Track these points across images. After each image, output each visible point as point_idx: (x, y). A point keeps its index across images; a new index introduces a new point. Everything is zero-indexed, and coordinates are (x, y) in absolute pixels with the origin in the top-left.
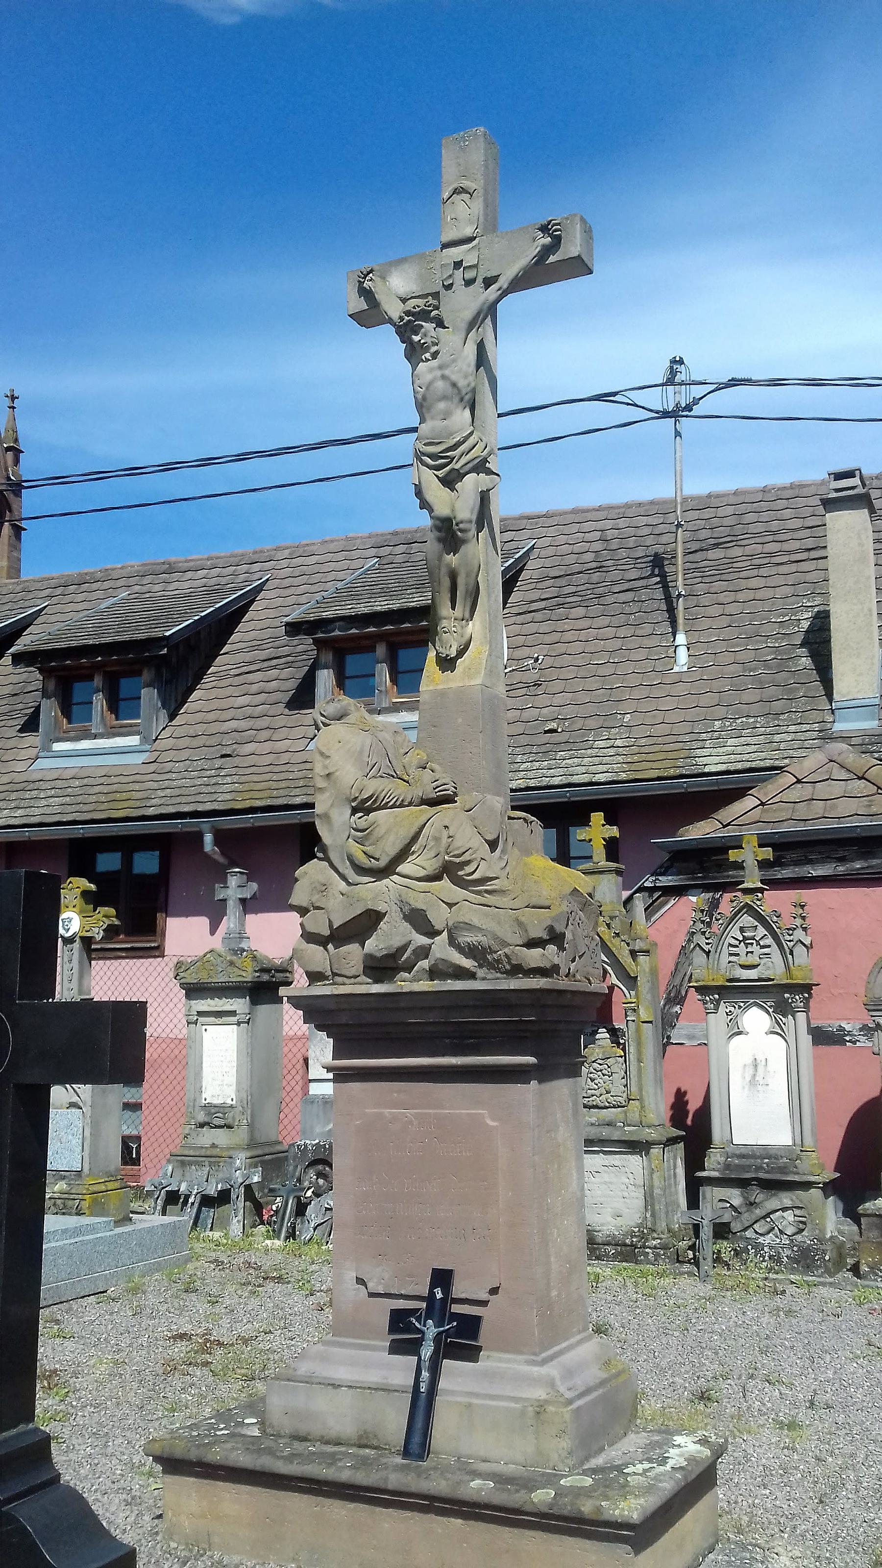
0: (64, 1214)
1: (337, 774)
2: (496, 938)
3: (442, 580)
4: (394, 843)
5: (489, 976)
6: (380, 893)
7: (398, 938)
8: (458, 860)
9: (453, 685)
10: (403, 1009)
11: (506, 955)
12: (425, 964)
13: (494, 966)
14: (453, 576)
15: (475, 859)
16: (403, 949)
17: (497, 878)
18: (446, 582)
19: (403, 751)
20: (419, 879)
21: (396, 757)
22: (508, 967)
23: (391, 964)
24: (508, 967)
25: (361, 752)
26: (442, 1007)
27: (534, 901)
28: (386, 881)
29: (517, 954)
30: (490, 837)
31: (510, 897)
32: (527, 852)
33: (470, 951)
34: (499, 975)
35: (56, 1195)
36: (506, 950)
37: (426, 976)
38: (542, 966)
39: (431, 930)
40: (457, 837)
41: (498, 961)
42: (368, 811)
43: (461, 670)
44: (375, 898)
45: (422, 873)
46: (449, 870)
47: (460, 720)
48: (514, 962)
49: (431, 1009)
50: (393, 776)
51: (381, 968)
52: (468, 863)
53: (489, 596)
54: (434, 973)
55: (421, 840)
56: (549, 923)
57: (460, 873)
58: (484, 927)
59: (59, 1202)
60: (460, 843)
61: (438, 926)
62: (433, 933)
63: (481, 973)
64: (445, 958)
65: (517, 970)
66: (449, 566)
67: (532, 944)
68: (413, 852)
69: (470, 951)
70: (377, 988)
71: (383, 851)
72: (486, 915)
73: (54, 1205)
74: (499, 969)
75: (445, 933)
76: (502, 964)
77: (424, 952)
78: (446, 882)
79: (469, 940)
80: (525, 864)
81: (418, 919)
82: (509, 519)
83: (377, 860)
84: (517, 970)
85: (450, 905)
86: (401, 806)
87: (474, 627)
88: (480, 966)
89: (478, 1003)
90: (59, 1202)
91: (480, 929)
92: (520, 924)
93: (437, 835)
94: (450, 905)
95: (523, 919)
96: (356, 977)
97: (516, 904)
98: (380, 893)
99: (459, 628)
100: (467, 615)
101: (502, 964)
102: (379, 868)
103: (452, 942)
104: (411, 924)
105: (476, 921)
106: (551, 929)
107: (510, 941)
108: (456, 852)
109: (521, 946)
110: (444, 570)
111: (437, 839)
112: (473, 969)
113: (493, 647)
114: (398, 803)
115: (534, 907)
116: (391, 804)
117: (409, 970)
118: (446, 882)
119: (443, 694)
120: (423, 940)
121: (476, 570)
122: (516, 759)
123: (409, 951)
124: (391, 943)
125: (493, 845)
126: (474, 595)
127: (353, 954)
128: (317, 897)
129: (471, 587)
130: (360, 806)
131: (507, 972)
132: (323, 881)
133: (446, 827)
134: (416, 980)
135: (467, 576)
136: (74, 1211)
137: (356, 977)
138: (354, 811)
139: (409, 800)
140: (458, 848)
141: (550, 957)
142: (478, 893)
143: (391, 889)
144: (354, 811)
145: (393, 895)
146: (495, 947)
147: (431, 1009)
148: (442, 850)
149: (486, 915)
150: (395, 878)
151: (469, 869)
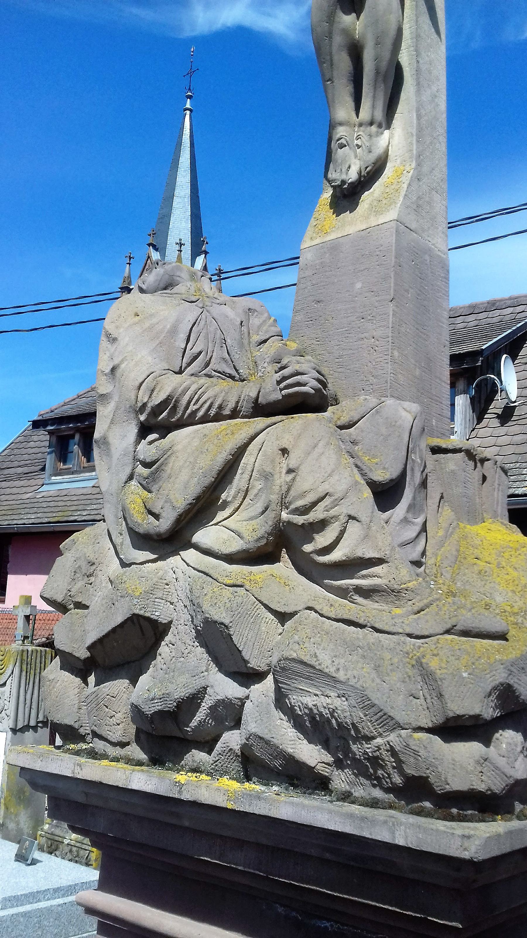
0: (76, 862)
1: (123, 366)
2: (368, 705)
3: (336, 58)
4: (186, 486)
5: (358, 792)
6: (172, 585)
7: (182, 680)
8: (300, 520)
9: (351, 230)
10: (187, 829)
11: (393, 751)
12: (232, 739)
13: (368, 768)
14: (355, 52)
15: (336, 518)
16: (192, 702)
17: (380, 561)
18: (343, 62)
19: (256, 338)
20: (230, 559)
21: (241, 345)
22: (398, 780)
23: (171, 730)
24: (398, 780)
25: (173, 331)
26: (258, 846)
27: (466, 619)
28: (174, 561)
29: (416, 753)
30: (381, 476)
31: (409, 607)
32: (474, 516)
33: (315, 727)
34: (378, 793)
35: (73, 843)
36: (393, 737)
37: (236, 766)
38: (482, 787)
39: (244, 670)
40: (304, 471)
41: (375, 761)
42: (165, 430)
43: (366, 206)
44: (150, 592)
45: (235, 546)
46: (280, 543)
47: (359, 285)
48: (410, 771)
49: (240, 844)
50: (232, 377)
51: (166, 735)
52: (321, 525)
53: (418, 92)
54: (253, 764)
55: (239, 480)
56: (501, 676)
57: (308, 548)
58: (341, 676)
59: (74, 849)
60: (309, 484)
61: (256, 663)
62: (248, 676)
63: (341, 780)
64: (267, 737)
65: (416, 791)
66: (347, 33)
67: (455, 729)
68: (225, 504)
69: (315, 727)
70: (144, 780)
71: (168, 500)
72: (352, 647)
73: (71, 851)
74: (378, 778)
75: (270, 677)
76: (383, 767)
77: (230, 714)
78: (284, 568)
79: (309, 701)
80: (465, 537)
81: (215, 640)
82: (522, 297)
83: (157, 517)
84: (416, 791)
85: (283, 617)
86: (218, 418)
87: (395, 140)
88: (339, 764)
89: (327, 856)
90: (74, 849)
91: (332, 680)
92: (427, 676)
93: (268, 469)
94: (283, 617)
95: (433, 664)
96: (123, 745)
97: (425, 624)
98: (172, 585)
99: (365, 138)
100: (379, 115)
101: (383, 767)
102: (159, 535)
103: (280, 700)
104: (209, 652)
105: (325, 661)
106: (506, 694)
107: (400, 716)
108: (300, 503)
109: (429, 731)
110: (338, 40)
111: (267, 477)
112: (322, 769)
113: (425, 169)
114: (212, 412)
115: (466, 633)
116: (201, 413)
117: (208, 745)
118: (284, 568)
119: (334, 248)
120: (226, 688)
121: (392, 33)
122: (522, 471)
123: (201, 715)
124: (171, 688)
125: (386, 494)
126: (394, 81)
127: (122, 698)
128: (80, 584)
129: (384, 64)
130: (152, 421)
131: (392, 790)
132: (92, 558)
133: (284, 451)
134: (215, 773)
135: (377, 44)
136: (84, 861)
137: (123, 745)
138: (144, 430)
139: (231, 405)
140: (303, 495)
141: (502, 762)
142: (342, 593)
143: (180, 575)
144: (144, 430)
145: (179, 592)
146: (368, 728)
147: (240, 844)
148: (275, 498)
149: (352, 647)
150: (190, 554)
151: (322, 539)
